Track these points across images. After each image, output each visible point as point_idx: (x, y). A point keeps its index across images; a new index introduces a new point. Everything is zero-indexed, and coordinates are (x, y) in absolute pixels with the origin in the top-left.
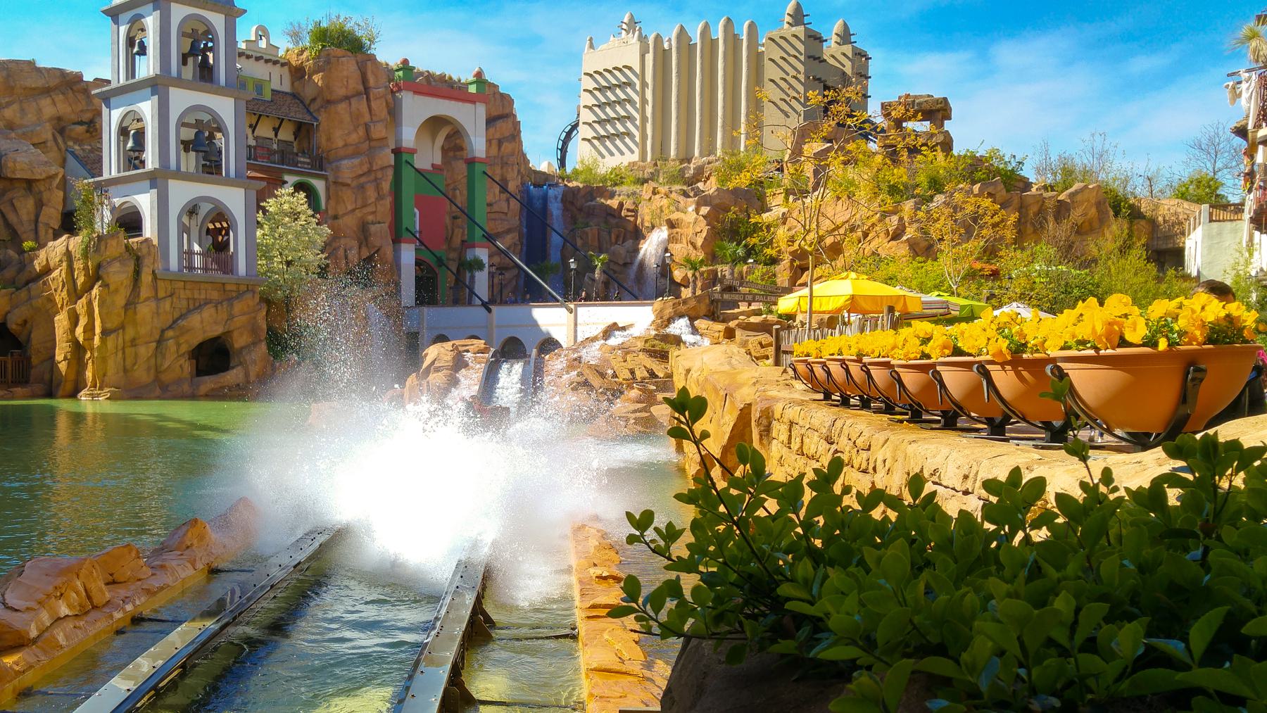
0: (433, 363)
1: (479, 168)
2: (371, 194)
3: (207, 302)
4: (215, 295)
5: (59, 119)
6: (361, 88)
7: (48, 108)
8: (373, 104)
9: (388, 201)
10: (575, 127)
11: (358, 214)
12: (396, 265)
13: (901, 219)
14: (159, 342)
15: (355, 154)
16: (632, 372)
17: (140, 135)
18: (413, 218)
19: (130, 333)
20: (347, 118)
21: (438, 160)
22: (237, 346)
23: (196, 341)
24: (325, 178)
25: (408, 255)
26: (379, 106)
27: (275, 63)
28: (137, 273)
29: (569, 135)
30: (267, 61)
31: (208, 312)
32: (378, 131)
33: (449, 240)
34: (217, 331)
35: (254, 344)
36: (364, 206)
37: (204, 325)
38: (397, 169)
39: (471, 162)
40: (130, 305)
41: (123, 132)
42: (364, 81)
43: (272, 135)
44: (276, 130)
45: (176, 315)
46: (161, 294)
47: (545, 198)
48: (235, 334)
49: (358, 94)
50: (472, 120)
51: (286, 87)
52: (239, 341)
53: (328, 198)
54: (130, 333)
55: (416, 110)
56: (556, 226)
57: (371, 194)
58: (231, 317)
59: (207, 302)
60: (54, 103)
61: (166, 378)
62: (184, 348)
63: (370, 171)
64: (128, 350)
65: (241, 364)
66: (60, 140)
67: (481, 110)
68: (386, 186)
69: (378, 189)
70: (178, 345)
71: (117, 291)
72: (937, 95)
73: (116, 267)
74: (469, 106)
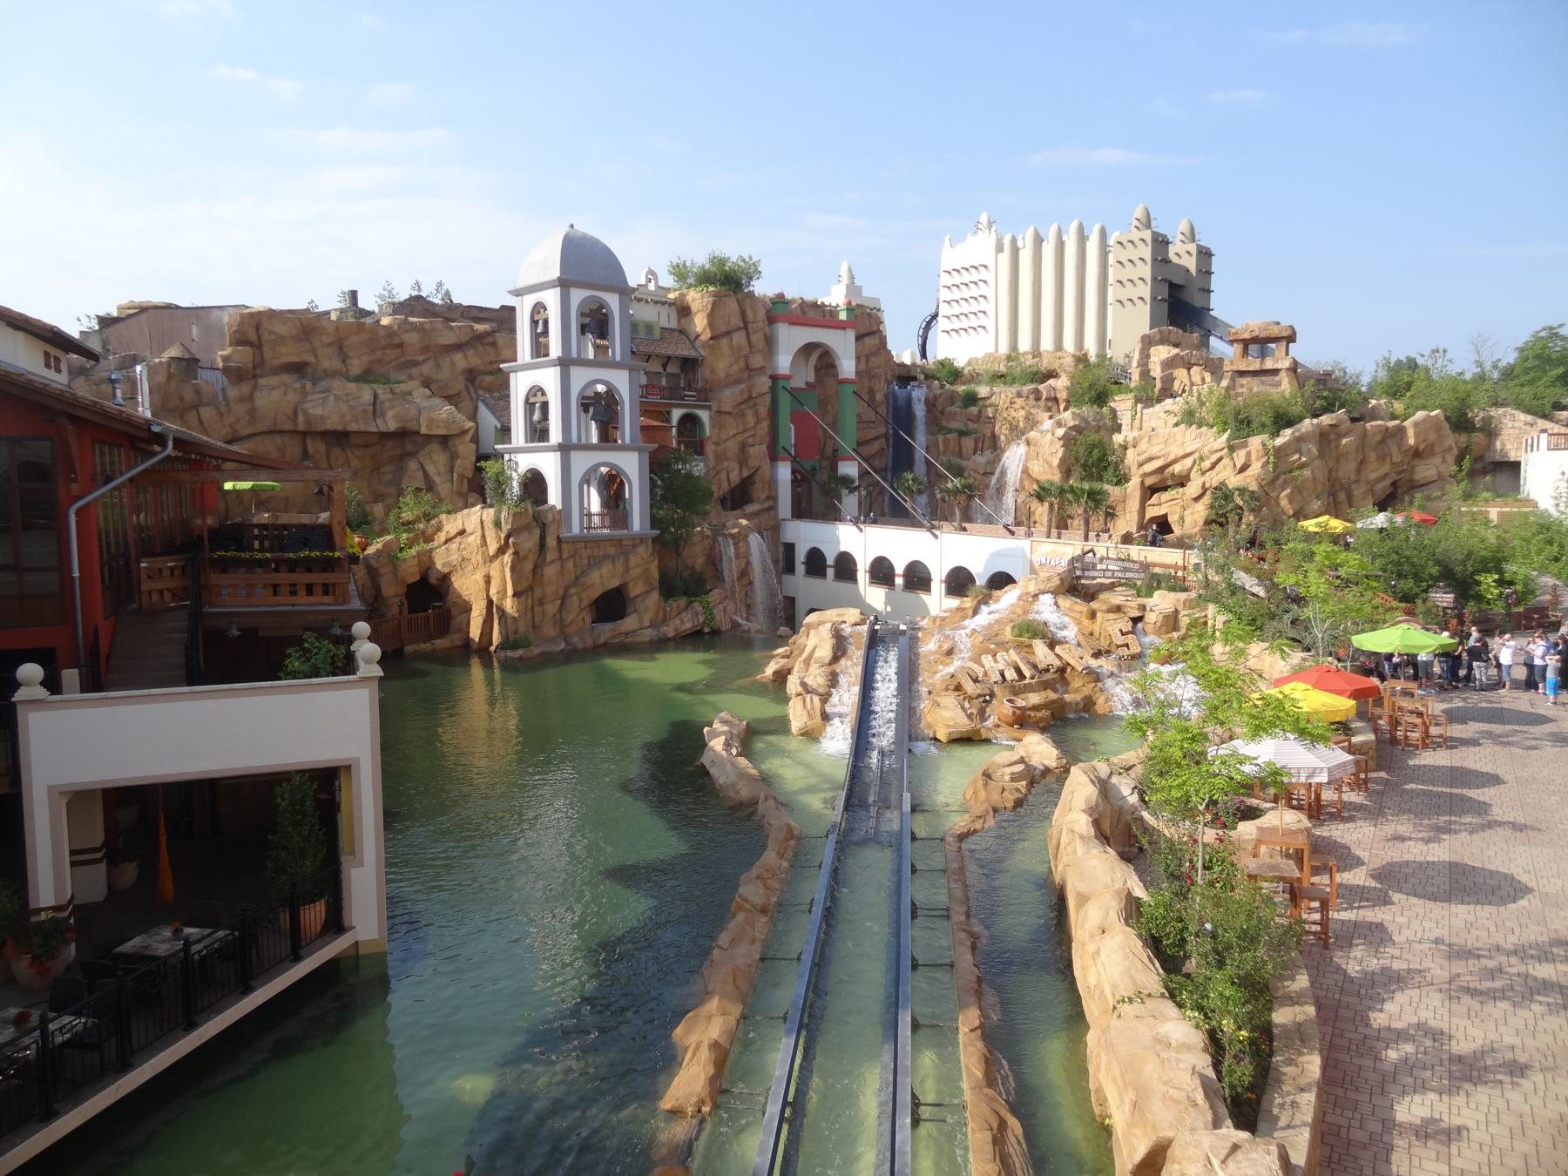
0: (813, 651)
2: (751, 419)
3: (605, 557)
4: (612, 551)
7: (460, 361)
8: (754, 338)
9: (765, 425)
10: (935, 317)
11: (740, 438)
12: (772, 483)
13: (1249, 454)
14: (564, 598)
15: (738, 381)
16: (1002, 675)
17: (545, 405)
18: (789, 435)
21: (811, 378)
22: (632, 595)
23: (596, 593)
24: (709, 408)
25: (784, 472)
26: (757, 339)
27: (663, 303)
28: (543, 538)
29: (929, 324)
30: (656, 302)
31: (606, 568)
34: (616, 583)
35: (647, 592)
37: (603, 579)
38: (773, 390)
43: (661, 370)
44: (665, 366)
45: (579, 571)
46: (565, 555)
47: (909, 400)
48: (631, 585)
49: (739, 329)
50: (844, 349)
51: (673, 324)
52: (635, 590)
53: (713, 426)
54: (538, 592)
55: (790, 339)
57: (751, 419)
58: (627, 570)
59: (605, 557)
62: (586, 603)
63: (750, 398)
64: (537, 609)
67: (851, 335)
68: (763, 410)
69: (756, 414)
70: (581, 600)
71: (525, 558)
72: (1285, 323)
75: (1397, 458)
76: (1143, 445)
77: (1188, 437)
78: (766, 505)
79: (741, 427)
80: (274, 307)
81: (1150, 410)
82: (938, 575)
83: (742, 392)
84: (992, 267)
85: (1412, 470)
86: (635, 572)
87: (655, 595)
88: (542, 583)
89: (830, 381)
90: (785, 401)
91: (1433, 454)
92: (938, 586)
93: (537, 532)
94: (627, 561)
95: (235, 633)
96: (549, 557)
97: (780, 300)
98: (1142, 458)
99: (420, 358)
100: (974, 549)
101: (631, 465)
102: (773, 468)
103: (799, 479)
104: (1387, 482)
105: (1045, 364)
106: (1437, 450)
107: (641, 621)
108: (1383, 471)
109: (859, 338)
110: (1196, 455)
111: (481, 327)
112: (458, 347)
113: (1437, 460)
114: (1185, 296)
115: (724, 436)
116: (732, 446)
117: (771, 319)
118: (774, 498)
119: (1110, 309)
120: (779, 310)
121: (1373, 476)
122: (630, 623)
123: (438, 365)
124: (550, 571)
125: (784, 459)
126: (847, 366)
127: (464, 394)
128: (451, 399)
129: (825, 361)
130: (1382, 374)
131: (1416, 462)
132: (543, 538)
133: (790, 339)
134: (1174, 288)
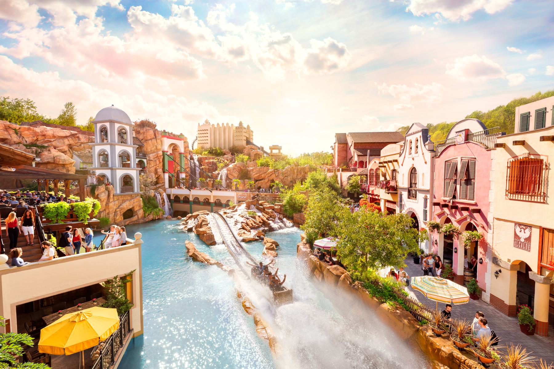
1: (182, 155)
3: (127, 200)
4: (129, 198)
5: (70, 145)
15: (154, 152)
19: (107, 211)
25: (167, 176)
28: (109, 196)
32: (159, 147)
34: (131, 207)
37: (127, 206)
38: (163, 155)
39: (180, 154)
40: (107, 204)
42: (155, 135)
50: (180, 144)
52: (136, 209)
54: (107, 211)
57: (158, 162)
61: (117, 222)
62: (122, 213)
68: (161, 160)
73: (103, 194)
80: (151, 121)
88: (108, 208)
93: (107, 193)
96: (111, 200)
99: (52, 140)
102: (164, 175)
115: (151, 166)
116: (153, 169)
118: (164, 183)
120: (166, 134)
124: (111, 205)
127: (68, 152)
129: (175, 147)
130: (237, 124)
133: (166, 144)
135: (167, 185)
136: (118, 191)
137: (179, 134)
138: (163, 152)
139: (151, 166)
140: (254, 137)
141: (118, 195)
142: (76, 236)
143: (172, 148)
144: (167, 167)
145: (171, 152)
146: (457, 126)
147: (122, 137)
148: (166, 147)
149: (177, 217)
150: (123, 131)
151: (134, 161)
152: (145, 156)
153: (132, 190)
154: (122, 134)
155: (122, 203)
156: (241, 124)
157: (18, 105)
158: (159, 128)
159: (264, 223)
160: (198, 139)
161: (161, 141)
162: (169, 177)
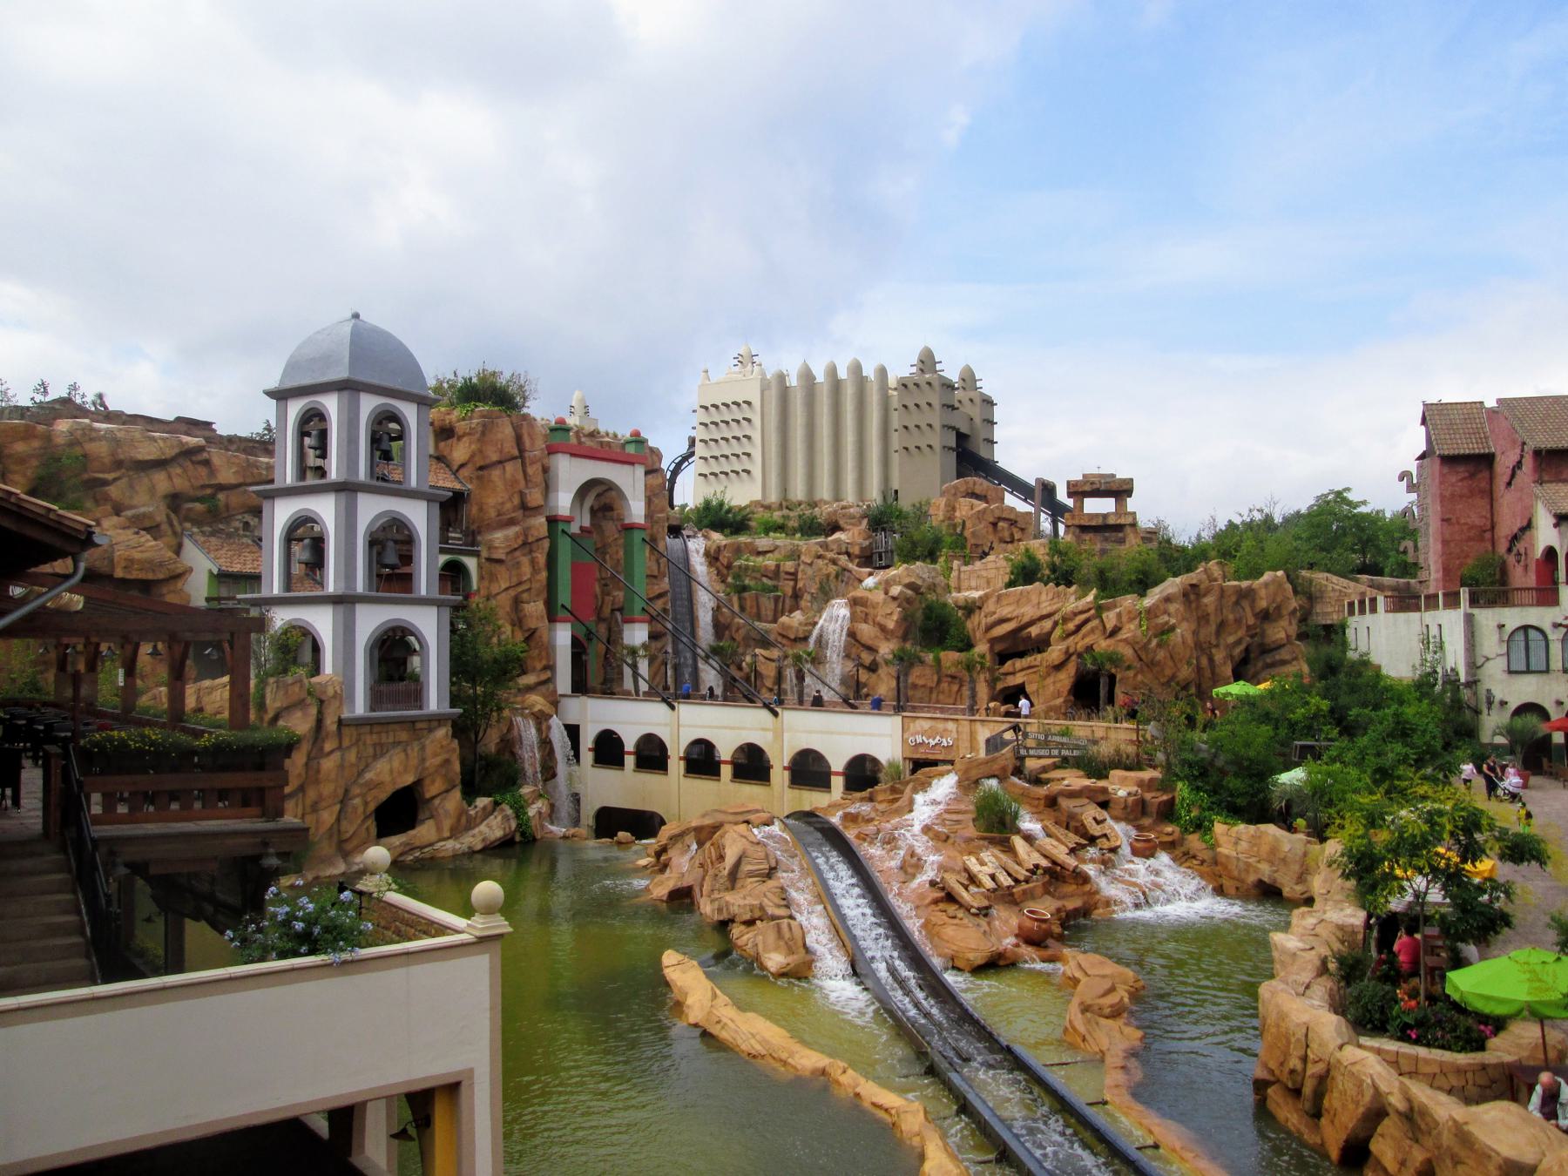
3: (397, 743)
4: (403, 736)
6: (516, 452)
8: (530, 471)
9: (544, 574)
11: (512, 593)
12: (549, 650)
13: (1119, 615)
15: (512, 522)
17: (318, 544)
20: (500, 484)
22: (428, 796)
24: (477, 554)
25: (563, 636)
32: (535, 497)
33: (599, 610)
34: (409, 779)
35: (447, 791)
36: (520, 583)
39: (630, 528)
41: (290, 537)
46: (346, 743)
48: (427, 782)
50: (631, 484)
53: (481, 578)
54: (312, 794)
55: (570, 474)
56: (700, 579)
57: (526, 570)
58: (423, 760)
60: (170, 478)
62: (372, 807)
63: (525, 544)
65: (432, 817)
66: (176, 523)
68: (541, 559)
70: (366, 804)
74: (627, 468)
75: (1251, 621)
76: (990, 606)
77: (1044, 597)
78: (543, 677)
79: (515, 581)
81: (969, 568)
82: (676, 752)
83: (517, 536)
84: (757, 403)
85: (1263, 634)
86: (433, 762)
87: (457, 794)
89: (610, 528)
90: (565, 546)
91: (1280, 616)
92: (676, 765)
93: (314, 711)
94: (423, 748)
95: (229, 933)
96: (328, 747)
97: (561, 428)
98: (991, 619)
99: (109, 476)
100: (790, 732)
101: (428, 624)
103: (579, 649)
104: (1242, 647)
105: (823, 513)
106: (1285, 612)
107: (439, 829)
108: (1240, 634)
109: (647, 473)
110: (1056, 617)
111: (192, 441)
112: (160, 464)
113: (1284, 623)
114: (971, 446)
117: (552, 451)
118: (550, 667)
119: (895, 459)
120: (562, 438)
121: (1231, 639)
122: (424, 832)
123: (131, 486)
125: (564, 621)
126: (637, 510)
128: (153, 530)
129: (601, 498)
131: (1266, 626)
132: (320, 722)
133: (570, 474)
134: (962, 437)
135: (564, 682)
136: (360, 707)
137: (625, 433)
138: (553, 521)
139: (495, 589)
140: (998, 434)
141: (359, 723)
142: (490, 742)
143: (589, 501)
144: (564, 596)
145: (587, 523)
146: (679, 479)
147: (387, 456)
148: (564, 501)
149: (612, 835)
150: (393, 426)
151: (425, 568)
152: (472, 541)
153: (416, 696)
154: (385, 438)
155: (375, 757)
156: (927, 361)
157: (483, 378)
158: (541, 409)
159: (1055, 875)
160: (700, 449)
161: (546, 470)
162: (576, 642)
